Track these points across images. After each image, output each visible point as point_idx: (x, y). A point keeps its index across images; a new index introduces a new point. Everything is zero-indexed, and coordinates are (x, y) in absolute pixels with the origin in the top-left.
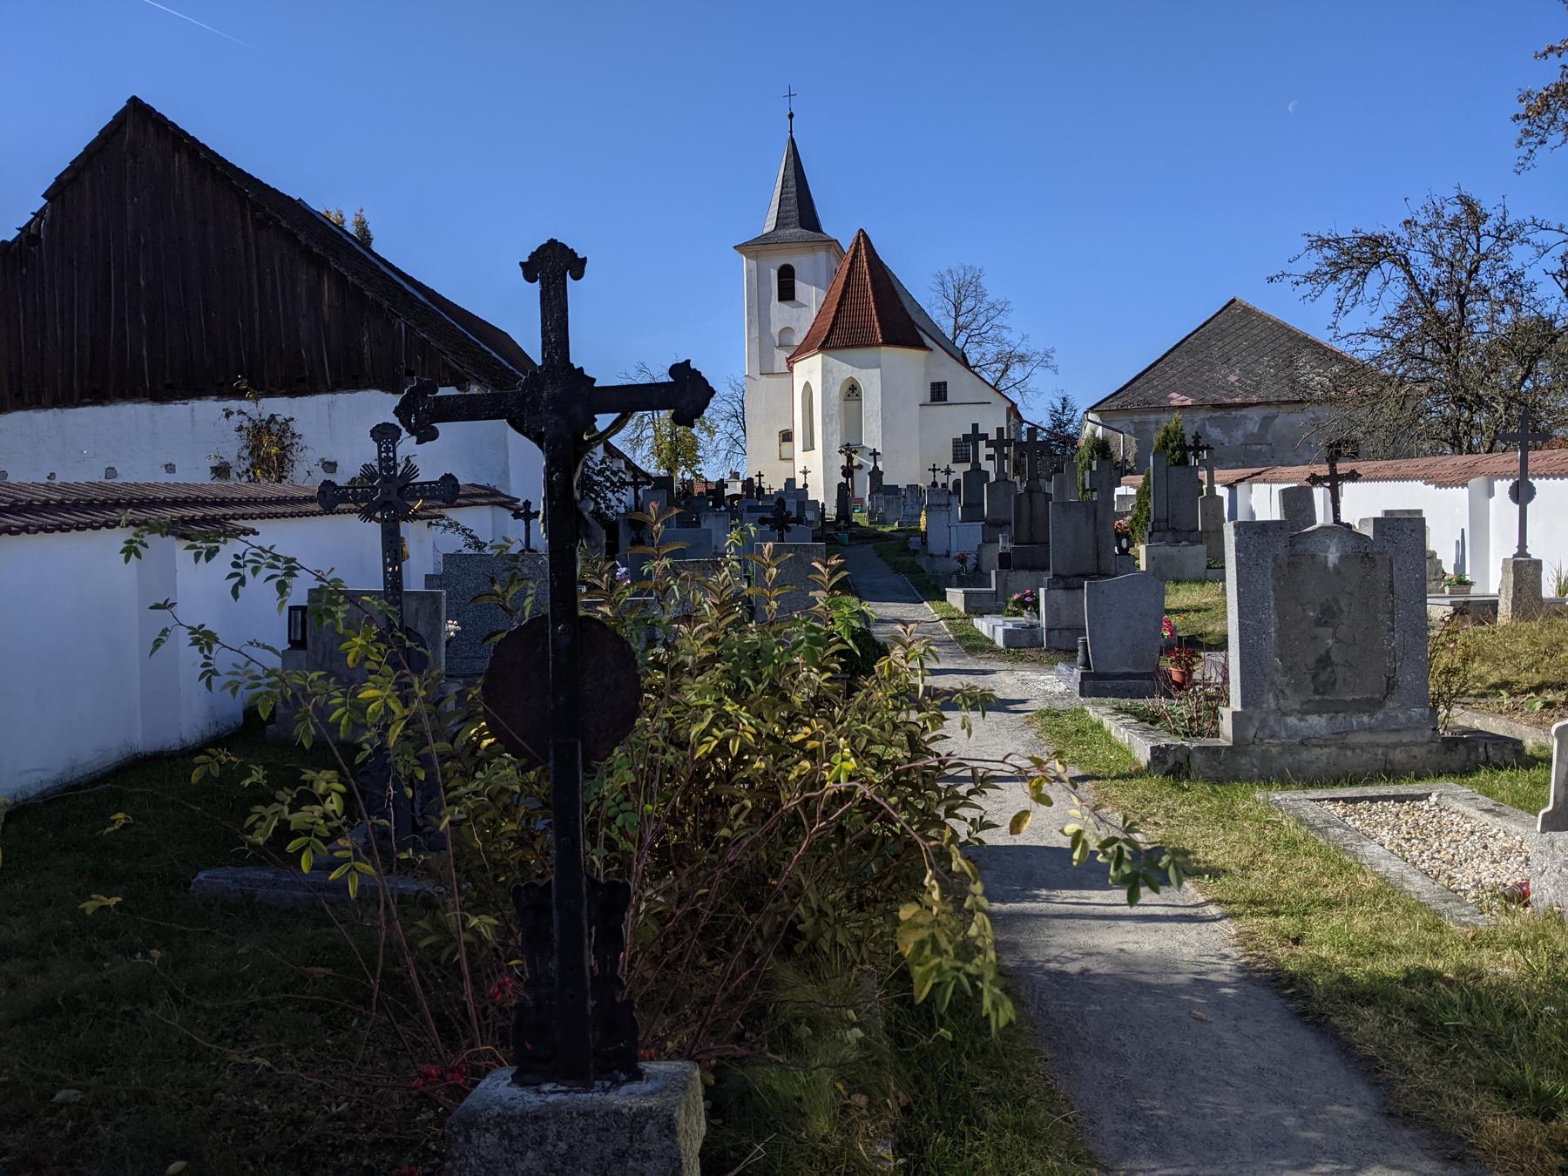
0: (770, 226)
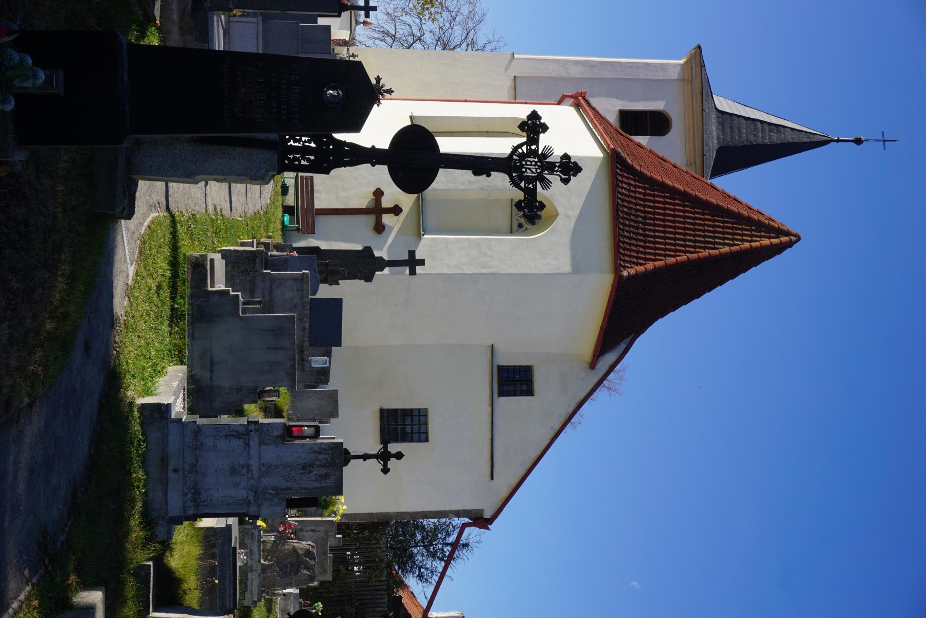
0: (723, 104)
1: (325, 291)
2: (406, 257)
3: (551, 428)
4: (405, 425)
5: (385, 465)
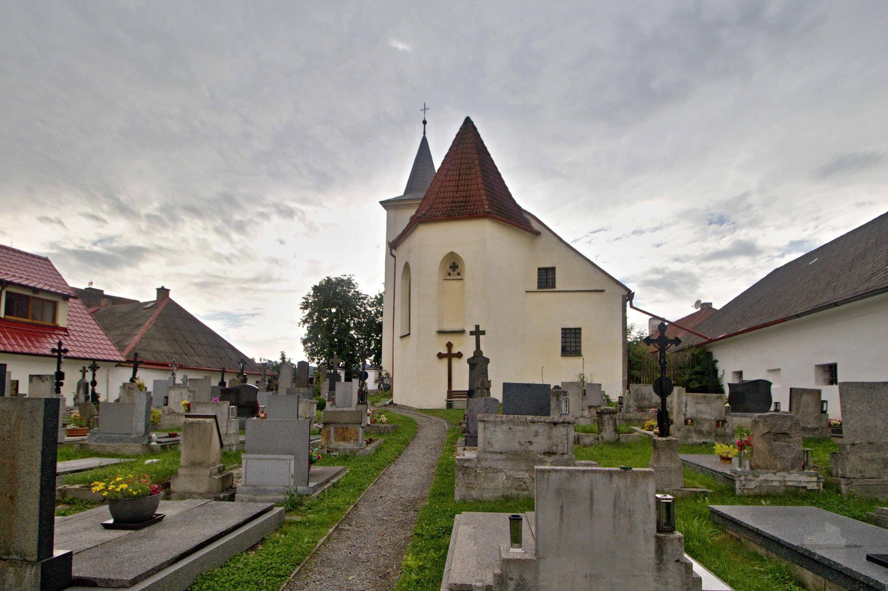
1: (497, 393)
2: (474, 337)
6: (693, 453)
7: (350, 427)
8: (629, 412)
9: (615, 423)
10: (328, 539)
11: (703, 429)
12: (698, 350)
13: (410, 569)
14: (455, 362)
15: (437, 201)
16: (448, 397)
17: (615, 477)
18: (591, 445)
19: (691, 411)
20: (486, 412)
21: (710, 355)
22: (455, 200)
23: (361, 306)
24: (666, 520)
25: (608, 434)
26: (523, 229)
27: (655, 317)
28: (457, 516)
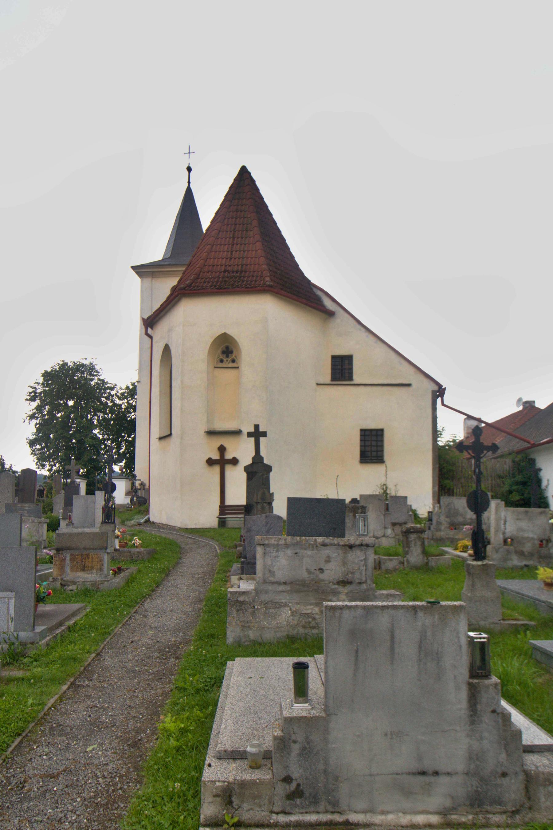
1: (280, 508)
2: (252, 439)
3: (376, 343)
4: (371, 445)
5: (488, 448)
6: (513, 578)
7: (92, 553)
8: (440, 530)
9: (423, 544)
10: (61, 699)
11: (524, 550)
12: (519, 457)
13: (168, 734)
14: (229, 470)
15: (206, 269)
16: (220, 514)
17: (421, 614)
18: (395, 570)
19: (511, 529)
20: (268, 532)
21: (532, 462)
22: (229, 268)
23: (107, 398)
24: (480, 663)
25: (415, 556)
26: (310, 306)
27: (469, 417)
28: (229, 663)
